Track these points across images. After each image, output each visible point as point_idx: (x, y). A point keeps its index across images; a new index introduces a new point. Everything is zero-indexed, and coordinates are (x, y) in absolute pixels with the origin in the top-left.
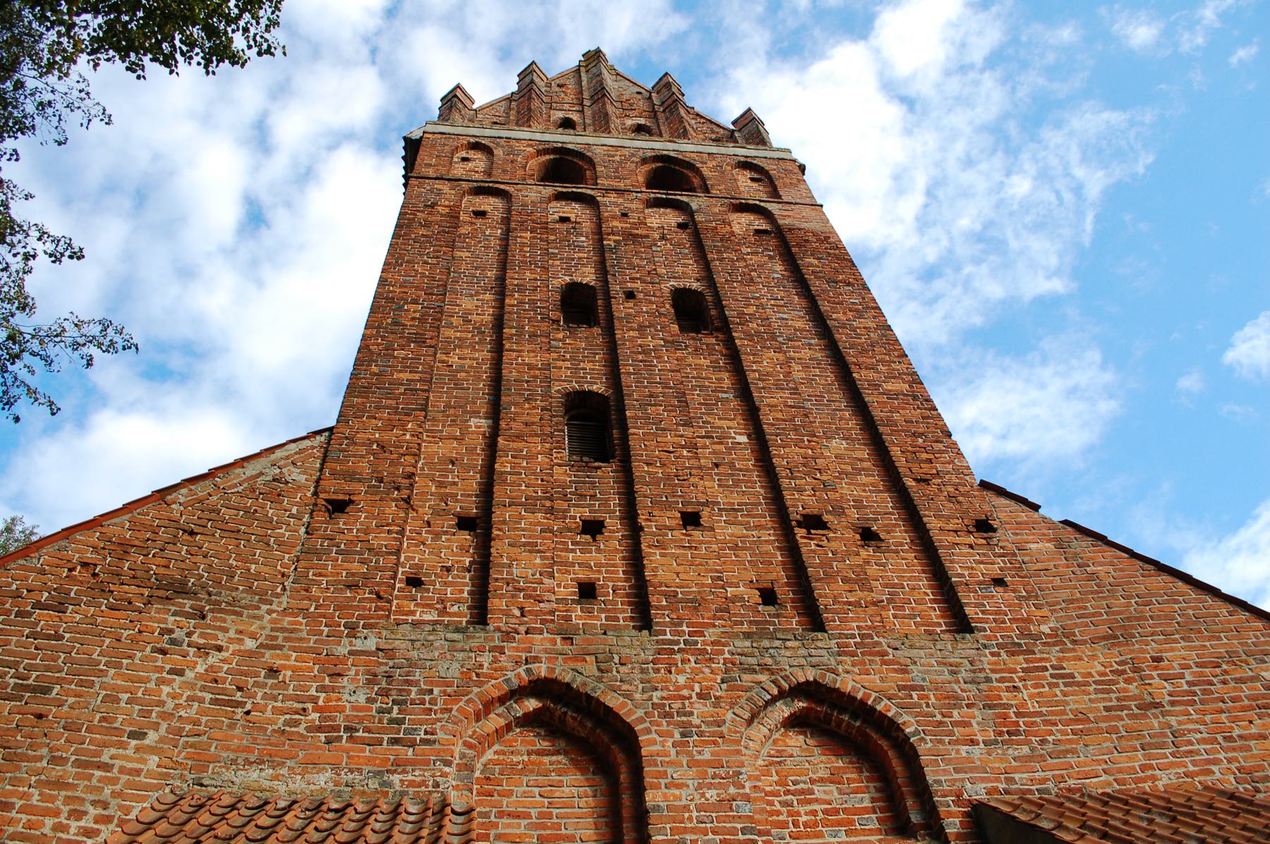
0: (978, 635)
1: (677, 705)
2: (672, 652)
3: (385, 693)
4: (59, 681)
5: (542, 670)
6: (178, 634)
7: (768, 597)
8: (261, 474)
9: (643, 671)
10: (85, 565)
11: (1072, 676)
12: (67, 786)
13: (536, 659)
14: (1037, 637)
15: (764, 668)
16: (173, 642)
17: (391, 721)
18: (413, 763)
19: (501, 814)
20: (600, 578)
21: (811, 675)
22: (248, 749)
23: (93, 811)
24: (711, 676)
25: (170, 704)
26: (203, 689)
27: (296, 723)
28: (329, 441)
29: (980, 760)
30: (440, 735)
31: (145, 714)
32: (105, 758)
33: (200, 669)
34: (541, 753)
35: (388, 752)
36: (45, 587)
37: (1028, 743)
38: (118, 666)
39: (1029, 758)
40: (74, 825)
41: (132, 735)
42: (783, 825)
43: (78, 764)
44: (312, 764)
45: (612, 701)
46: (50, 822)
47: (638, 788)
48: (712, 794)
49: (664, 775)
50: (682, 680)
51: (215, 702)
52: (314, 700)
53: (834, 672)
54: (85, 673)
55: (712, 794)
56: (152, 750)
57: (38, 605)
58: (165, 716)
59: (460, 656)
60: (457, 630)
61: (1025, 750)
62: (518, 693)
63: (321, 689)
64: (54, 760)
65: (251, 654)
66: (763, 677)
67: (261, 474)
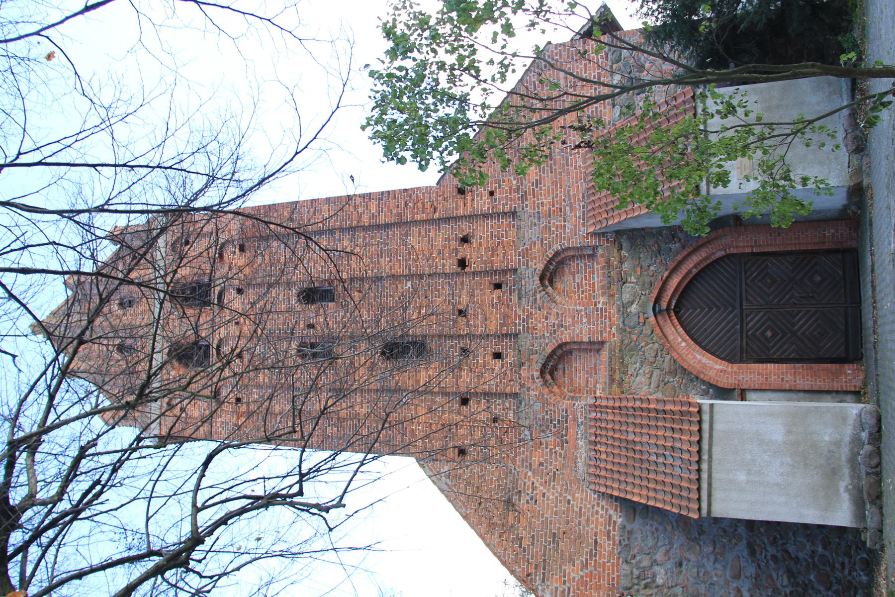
0: (517, 210)
1: (550, 328)
2: (528, 327)
3: (547, 427)
4: (550, 531)
5: (537, 374)
6: (528, 498)
7: (498, 286)
8: (446, 483)
9: (536, 338)
10: (500, 536)
11: (537, 180)
12: (588, 519)
13: (532, 376)
14: (518, 188)
15: (534, 295)
16: (532, 499)
17: (559, 423)
18: (574, 415)
19: (587, 386)
20: (491, 350)
21: (537, 278)
22: (571, 467)
23: (596, 508)
24: (538, 314)
25: (556, 494)
26: (549, 485)
27: (560, 454)
28: (427, 458)
29: (414, 71)
30: (564, 407)
31: (561, 501)
32: (578, 510)
33: (542, 488)
34: (564, 373)
35: (571, 422)
36: (513, 547)
37: (565, 206)
38: (543, 514)
39: (571, 207)
40: (601, 512)
41: (569, 503)
42: (590, 294)
43: (580, 517)
44: (576, 447)
45: (549, 350)
46: (600, 520)
47: (581, 343)
48: (584, 320)
49: (577, 335)
50: (540, 325)
51: (554, 481)
52: (551, 449)
53: (535, 269)
54: (545, 523)
55: (584, 320)
56: (574, 496)
57: (520, 546)
58: (561, 495)
59: (532, 402)
60: (521, 403)
61: (567, 208)
62: (545, 382)
63: (547, 448)
64: (580, 524)
65: (534, 473)
66: (538, 296)
67: (446, 483)
